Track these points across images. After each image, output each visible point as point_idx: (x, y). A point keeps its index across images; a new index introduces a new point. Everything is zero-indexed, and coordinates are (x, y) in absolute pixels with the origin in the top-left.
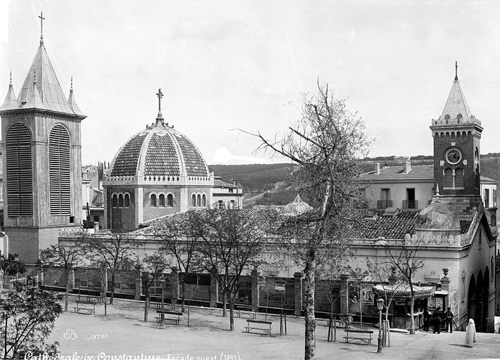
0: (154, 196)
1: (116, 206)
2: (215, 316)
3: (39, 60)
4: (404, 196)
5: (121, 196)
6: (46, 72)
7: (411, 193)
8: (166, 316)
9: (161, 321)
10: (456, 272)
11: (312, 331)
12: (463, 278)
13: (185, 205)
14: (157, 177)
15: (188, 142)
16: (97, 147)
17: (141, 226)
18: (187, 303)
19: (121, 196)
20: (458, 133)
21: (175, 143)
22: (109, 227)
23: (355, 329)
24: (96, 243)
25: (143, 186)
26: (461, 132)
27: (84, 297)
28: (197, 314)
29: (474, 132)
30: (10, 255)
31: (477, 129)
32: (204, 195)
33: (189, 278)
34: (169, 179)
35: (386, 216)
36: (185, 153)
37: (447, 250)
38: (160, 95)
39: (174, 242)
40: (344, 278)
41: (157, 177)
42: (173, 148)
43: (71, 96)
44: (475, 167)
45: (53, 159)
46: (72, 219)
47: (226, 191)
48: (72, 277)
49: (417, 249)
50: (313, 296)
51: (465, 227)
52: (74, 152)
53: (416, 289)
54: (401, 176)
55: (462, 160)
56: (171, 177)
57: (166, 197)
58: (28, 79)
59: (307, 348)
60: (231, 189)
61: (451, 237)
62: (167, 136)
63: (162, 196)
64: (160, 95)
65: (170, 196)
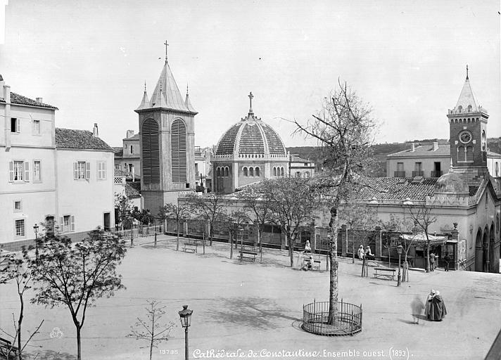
0: (245, 169)
1: (221, 176)
2: (282, 256)
3: (164, 74)
4: (432, 168)
5: (223, 168)
6: (170, 84)
7: (438, 165)
8: (244, 255)
9: (241, 259)
10: (466, 227)
11: (335, 270)
12: (471, 231)
13: (268, 174)
14: (248, 155)
15: (271, 130)
16: (206, 135)
17: (237, 190)
18: (264, 246)
19: (223, 168)
20: (469, 119)
21: (261, 130)
22: (215, 191)
23: (385, 268)
24: (200, 203)
25: (238, 162)
26: (471, 118)
27: (192, 240)
28: (270, 255)
29: (481, 118)
30: (143, 211)
31: (483, 116)
32: (282, 168)
33: (266, 228)
34: (256, 156)
35: (415, 183)
36: (268, 138)
37: (458, 208)
38: (251, 96)
39: (253, 202)
40: (378, 229)
41: (248, 155)
42: (260, 134)
43: (187, 99)
44: (482, 145)
45: (174, 144)
46: (188, 186)
47: (303, 165)
48: (186, 225)
49: (433, 207)
50: (336, 243)
51: (473, 191)
52: (188, 138)
53: (431, 238)
54: (430, 153)
55: (472, 140)
56: (258, 155)
57: (254, 169)
58: (157, 87)
59: (331, 282)
60: (306, 164)
61: (461, 198)
62: (256, 126)
63: (251, 169)
64: (251, 96)
65: (257, 169)
